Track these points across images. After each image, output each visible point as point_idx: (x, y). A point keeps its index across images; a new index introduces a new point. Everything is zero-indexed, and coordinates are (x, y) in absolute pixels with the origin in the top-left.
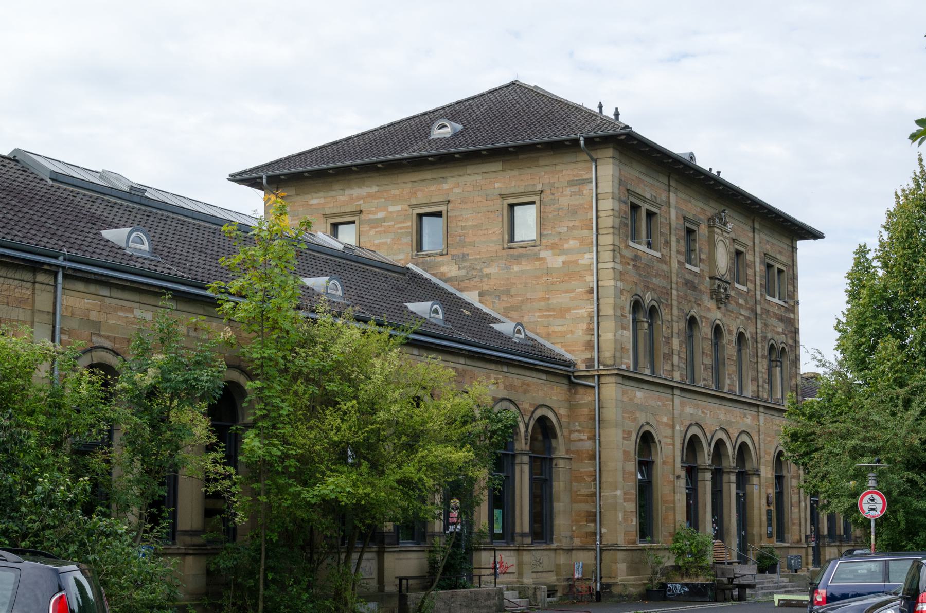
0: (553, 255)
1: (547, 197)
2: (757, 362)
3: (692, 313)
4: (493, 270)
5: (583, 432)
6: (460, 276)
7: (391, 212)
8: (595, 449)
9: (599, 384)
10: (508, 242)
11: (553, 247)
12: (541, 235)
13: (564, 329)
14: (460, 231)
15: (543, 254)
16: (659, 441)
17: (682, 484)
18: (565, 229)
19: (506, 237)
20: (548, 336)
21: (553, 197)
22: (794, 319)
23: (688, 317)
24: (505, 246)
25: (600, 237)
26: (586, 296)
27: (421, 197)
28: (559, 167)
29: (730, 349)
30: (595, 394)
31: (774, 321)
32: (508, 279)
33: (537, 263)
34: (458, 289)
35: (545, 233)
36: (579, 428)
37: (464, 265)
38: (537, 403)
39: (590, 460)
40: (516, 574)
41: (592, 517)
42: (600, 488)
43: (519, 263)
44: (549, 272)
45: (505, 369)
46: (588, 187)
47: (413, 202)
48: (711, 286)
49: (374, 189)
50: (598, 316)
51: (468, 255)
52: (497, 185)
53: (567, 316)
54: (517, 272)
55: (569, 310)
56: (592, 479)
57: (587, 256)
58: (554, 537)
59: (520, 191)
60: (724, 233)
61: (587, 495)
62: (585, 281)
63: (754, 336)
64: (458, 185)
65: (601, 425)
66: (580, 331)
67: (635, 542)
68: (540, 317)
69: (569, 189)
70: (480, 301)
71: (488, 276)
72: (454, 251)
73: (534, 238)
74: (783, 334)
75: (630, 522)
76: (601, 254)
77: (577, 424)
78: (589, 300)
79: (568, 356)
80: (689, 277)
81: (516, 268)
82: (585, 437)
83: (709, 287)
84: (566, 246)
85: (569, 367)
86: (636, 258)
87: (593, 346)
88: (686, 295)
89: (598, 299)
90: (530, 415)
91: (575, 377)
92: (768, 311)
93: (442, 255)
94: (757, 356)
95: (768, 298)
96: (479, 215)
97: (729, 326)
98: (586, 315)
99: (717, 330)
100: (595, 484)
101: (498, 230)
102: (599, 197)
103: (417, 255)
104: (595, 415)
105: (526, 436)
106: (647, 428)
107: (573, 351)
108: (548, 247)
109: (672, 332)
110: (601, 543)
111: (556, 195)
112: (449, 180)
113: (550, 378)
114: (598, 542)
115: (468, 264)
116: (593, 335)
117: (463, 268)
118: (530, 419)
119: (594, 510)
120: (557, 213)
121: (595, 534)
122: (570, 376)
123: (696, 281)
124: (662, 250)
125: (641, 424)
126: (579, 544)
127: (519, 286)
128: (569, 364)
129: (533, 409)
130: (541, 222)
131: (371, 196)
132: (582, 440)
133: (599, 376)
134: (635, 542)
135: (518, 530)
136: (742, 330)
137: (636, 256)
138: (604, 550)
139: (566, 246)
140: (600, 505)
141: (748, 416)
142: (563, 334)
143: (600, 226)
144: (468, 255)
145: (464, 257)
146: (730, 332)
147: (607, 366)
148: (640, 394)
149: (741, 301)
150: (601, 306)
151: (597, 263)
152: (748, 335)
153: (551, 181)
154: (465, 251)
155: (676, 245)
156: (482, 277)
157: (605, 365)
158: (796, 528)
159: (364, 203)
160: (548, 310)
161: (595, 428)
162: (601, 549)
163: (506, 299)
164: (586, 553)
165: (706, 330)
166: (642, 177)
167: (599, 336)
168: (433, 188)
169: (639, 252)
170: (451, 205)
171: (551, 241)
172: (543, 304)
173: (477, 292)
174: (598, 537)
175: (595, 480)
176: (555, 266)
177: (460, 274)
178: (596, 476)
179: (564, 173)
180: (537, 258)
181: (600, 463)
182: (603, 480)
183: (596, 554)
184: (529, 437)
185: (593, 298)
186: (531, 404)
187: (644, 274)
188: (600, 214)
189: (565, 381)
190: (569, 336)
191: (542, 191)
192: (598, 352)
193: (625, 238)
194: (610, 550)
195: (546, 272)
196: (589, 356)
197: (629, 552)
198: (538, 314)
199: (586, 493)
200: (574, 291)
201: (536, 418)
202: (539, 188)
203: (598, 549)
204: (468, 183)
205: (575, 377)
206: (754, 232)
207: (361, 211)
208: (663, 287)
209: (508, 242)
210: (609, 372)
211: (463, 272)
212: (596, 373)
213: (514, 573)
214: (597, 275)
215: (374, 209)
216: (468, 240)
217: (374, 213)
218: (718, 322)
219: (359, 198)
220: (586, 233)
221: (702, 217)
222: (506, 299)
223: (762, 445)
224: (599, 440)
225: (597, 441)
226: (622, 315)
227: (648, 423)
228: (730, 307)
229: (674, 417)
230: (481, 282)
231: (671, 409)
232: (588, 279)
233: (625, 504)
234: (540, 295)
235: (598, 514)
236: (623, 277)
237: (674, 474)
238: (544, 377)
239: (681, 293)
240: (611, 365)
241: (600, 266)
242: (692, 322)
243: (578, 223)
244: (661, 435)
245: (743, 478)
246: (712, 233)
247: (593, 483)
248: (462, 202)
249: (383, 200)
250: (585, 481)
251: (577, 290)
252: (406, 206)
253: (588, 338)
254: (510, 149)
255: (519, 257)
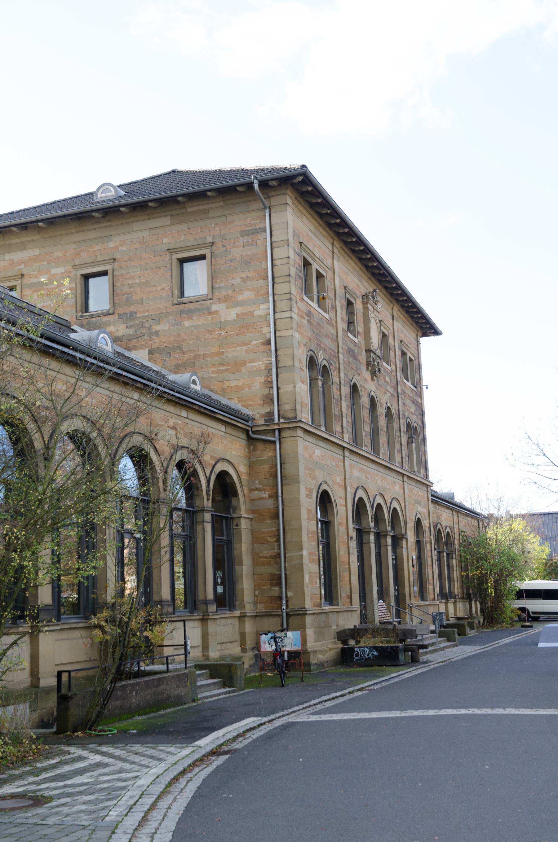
0: (227, 308)
1: (218, 249)
2: (400, 436)
3: (354, 380)
4: (162, 327)
5: (264, 490)
6: (127, 335)
7: (54, 275)
8: (278, 507)
9: (280, 439)
10: (178, 298)
11: (226, 299)
12: (213, 288)
13: (240, 383)
14: (128, 290)
15: (215, 308)
16: (335, 501)
17: (353, 544)
18: (239, 281)
19: (176, 292)
20: (223, 392)
21: (224, 249)
22: (421, 404)
23: (352, 384)
24: (175, 302)
25: (276, 285)
26: (263, 348)
27: (85, 257)
28: (230, 218)
29: (382, 421)
30: (275, 450)
31: (408, 402)
32: (179, 335)
33: (209, 317)
34: (126, 349)
35: (217, 286)
36: (259, 486)
37: (132, 323)
38: (218, 456)
39: (272, 519)
40: (201, 648)
41: (276, 580)
42: (285, 548)
43: (190, 318)
44: (222, 325)
45: (184, 414)
46: (261, 236)
47: (77, 262)
48: (367, 358)
49: (36, 252)
50: (277, 368)
51: (136, 313)
52: (165, 240)
53: (243, 369)
54: (188, 328)
55: (244, 363)
56: (275, 539)
57: (263, 306)
58: (237, 603)
59: (189, 245)
60: (375, 312)
61: (270, 557)
62: (261, 332)
63: (397, 412)
64: (124, 243)
65: (283, 482)
66: (258, 384)
67: (320, 605)
68: (213, 372)
69: (241, 240)
70: (150, 360)
71: (157, 333)
72: (121, 310)
73: (206, 292)
74: (415, 415)
75: (314, 584)
76: (278, 303)
77: (257, 482)
78: (266, 351)
79: (245, 411)
80: (351, 346)
81: (187, 323)
82: (266, 495)
83: (365, 359)
84: (240, 298)
85: (247, 421)
86: (309, 314)
87: (272, 400)
88: (349, 362)
89: (276, 350)
90: (211, 468)
91: (253, 432)
92: (405, 393)
93: (108, 314)
94: (400, 431)
95: (405, 381)
96: (147, 272)
97: (380, 400)
98: (263, 367)
99: (372, 401)
100: (279, 545)
101: (166, 285)
102: (274, 245)
103: (82, 316)
104: (276, 471)
105: (208, 491)
106: (324, 487)
107: (251, 406)
108: (220, 300)
109: (341, 395)
110: (287, 607)
111: (228, 247)
112: (114, 239)
113: (230, 430)
114: (284, 607)
115: (137, 322)
116: (272, 387)
117: (131, 327)
118: (211, 473)
119: (278, 573)
120: (230, 265)
121: (280, 598)
122: (248, 431)
123: (356, 351)
124: (330, 313)
125: (320, 483)
126: (263, 610)
127: (191, 342)
128: (246, 419)
129: (213, 463)
130: (213, 276)
131: (34, 259)
132: (263, 498)
133: (280, 430)
134: (320, 605)
135: (201, 597)
136: (389, 405)
137: (309, 312)
138: (291, 615)
139: (240, 298)
140: (285, 567)
141: (397, 484)
142: (239, 389)
143: (276, 275)
144: (136, 313)
145: (131, 316)
146: (381, 405)
147: (288, 419)
148: (318, 452)
149: (387, 379)
150: (280, 358)
151: (274, 314)
152: (393, 411)
153: (223, 233)
154: (133, 309)
155: (341, 313)
156: (151, 334)
157: (285, 418)
158: (431, 587)
159: (26, 266)
160: (223, 365)
161: (277, 485)
162: (287, 615)
163: (177, 356)
164: (271, 619)
165: (365, 400)
166: (311, 235)
167: (278, 388)
168: (97, 247)
169: (312, 309)
170: (117, 264)
171: (223, 294)
172: (216, 358)
173: (146, 351)
174: (284, 602)
175: (278, 540)
176: (229, 318)
177: (129, 333)
178: (279, 535)
179: (236, 224)
180: (209, 312)
181: (283, 522)
182: (288, 539)
183: (282, 620)
184: (211, 493)
185: (270, 349)
186: (211, 457)
187: (316, 331)
188: (276, 262)
189: (244, 436)
190: (246, 390)
191: (213, 243)
192: (278, 405)
193: (300, 291)
194: (298, 615)
195: (219, 326)
196: (268, 410)
197: (316, 616)
198: (212, 369)
199: (268, 555)
200: (250, 344)
201: (217, 472)
202: (210, 240)
203: (284, 615)
204: (135, 241)
205: (253, 432)
206: (393, 319)
207: (23, 275)
208: (331, 349)
209: (178, 298)
210: (290, 426)
211: (131, 331)
212: (276, 427)
213: (198, 646)
214: (275, 325)
215: (36, 273)
216: (135, 298)
217: (36, 277)
218: (373, 394)
219: (21, 262)
220: (261, 283)
221: (358, 293)
222: (177, 356)
223: (407, 511)
224: (282, 497)
225: (280, 499)
226: (301, 368)
227: (326, 482)
228: (382, 382)
229: (345, 479)
230: (151, 340)
231: (343, 470)
232: (265, 330)
233: (310, 565)
234: (214, 349)
235: (283, 575)
236: (299, 330)
237: (348, 535)
238: (223, 428)
239: (346, 359)
240: (292, 418)
241: (278, 315)
242: (354, 389)
243: (251, 274)
244: (336, 495)
245: (397, 540)
246: (366, 309)
247: (276, 544)
248: (129, 260)
249: (45, 263)
250: (268, 542)
251: (253, 343)
252: (69, 268)
253: (266, 391)
254: (179, 199)
255: (190, 313)
